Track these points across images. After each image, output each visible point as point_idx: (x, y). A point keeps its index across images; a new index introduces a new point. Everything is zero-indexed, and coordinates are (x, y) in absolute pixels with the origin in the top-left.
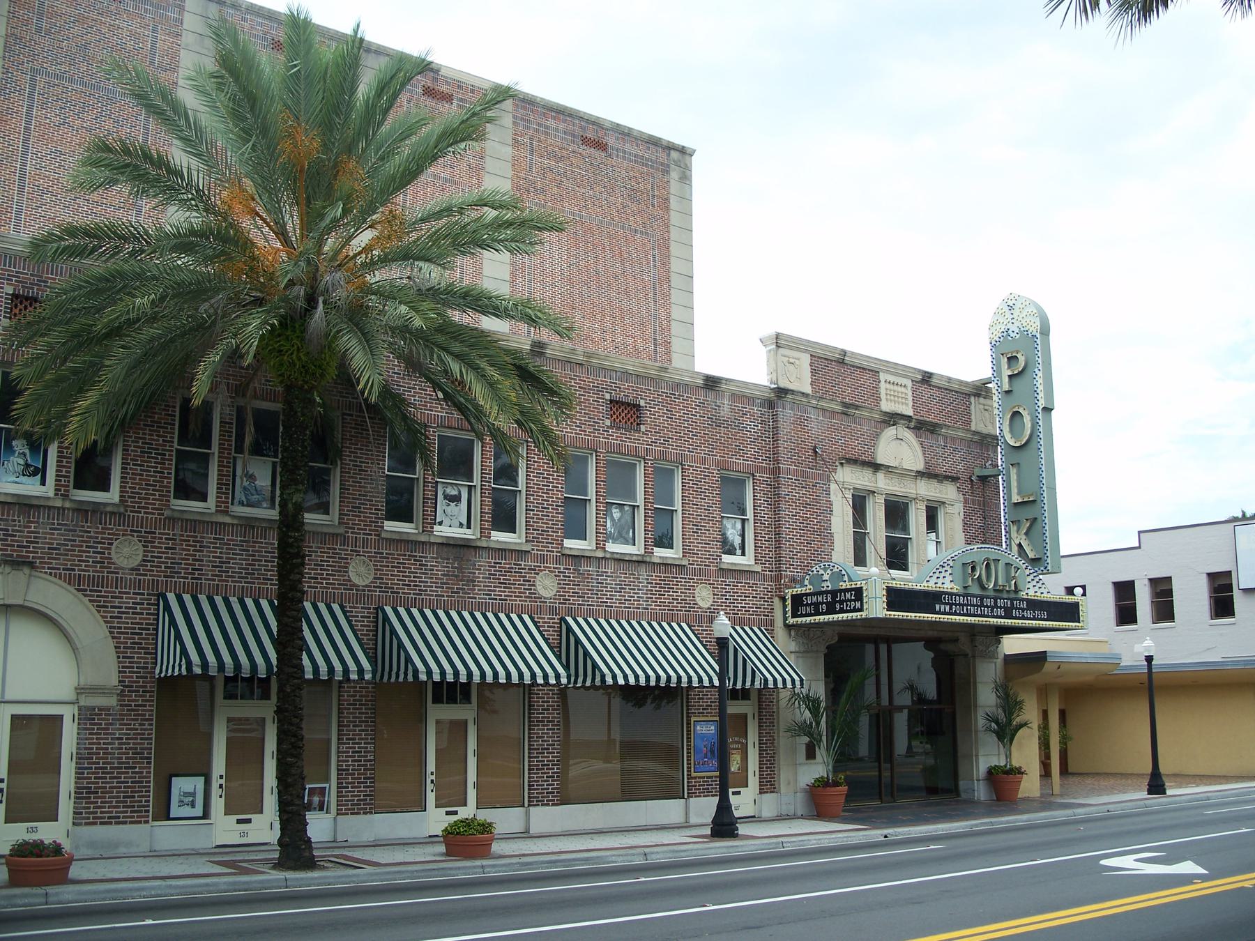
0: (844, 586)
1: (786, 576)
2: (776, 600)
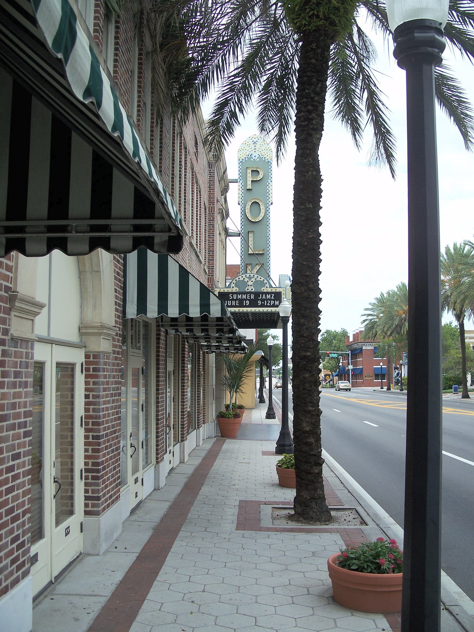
0: (264, 289)
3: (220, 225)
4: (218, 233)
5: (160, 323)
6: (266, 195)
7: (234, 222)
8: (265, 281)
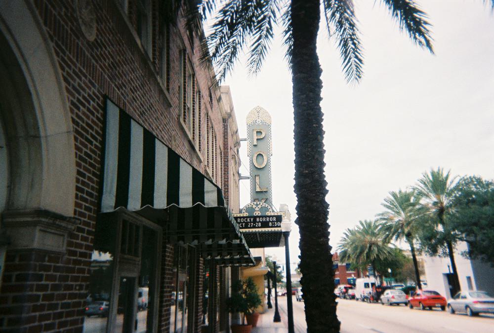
3: (234, 168)
4: (232, 173)
5: (200, 249)
6: (268, 149)
7: (245, 169)
8: (269, 207)
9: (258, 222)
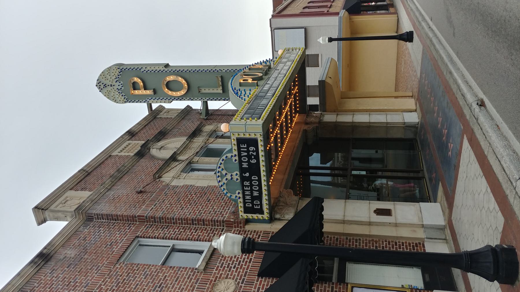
1: (229, 217)
2: (248, 227)
9: (253, 204)
